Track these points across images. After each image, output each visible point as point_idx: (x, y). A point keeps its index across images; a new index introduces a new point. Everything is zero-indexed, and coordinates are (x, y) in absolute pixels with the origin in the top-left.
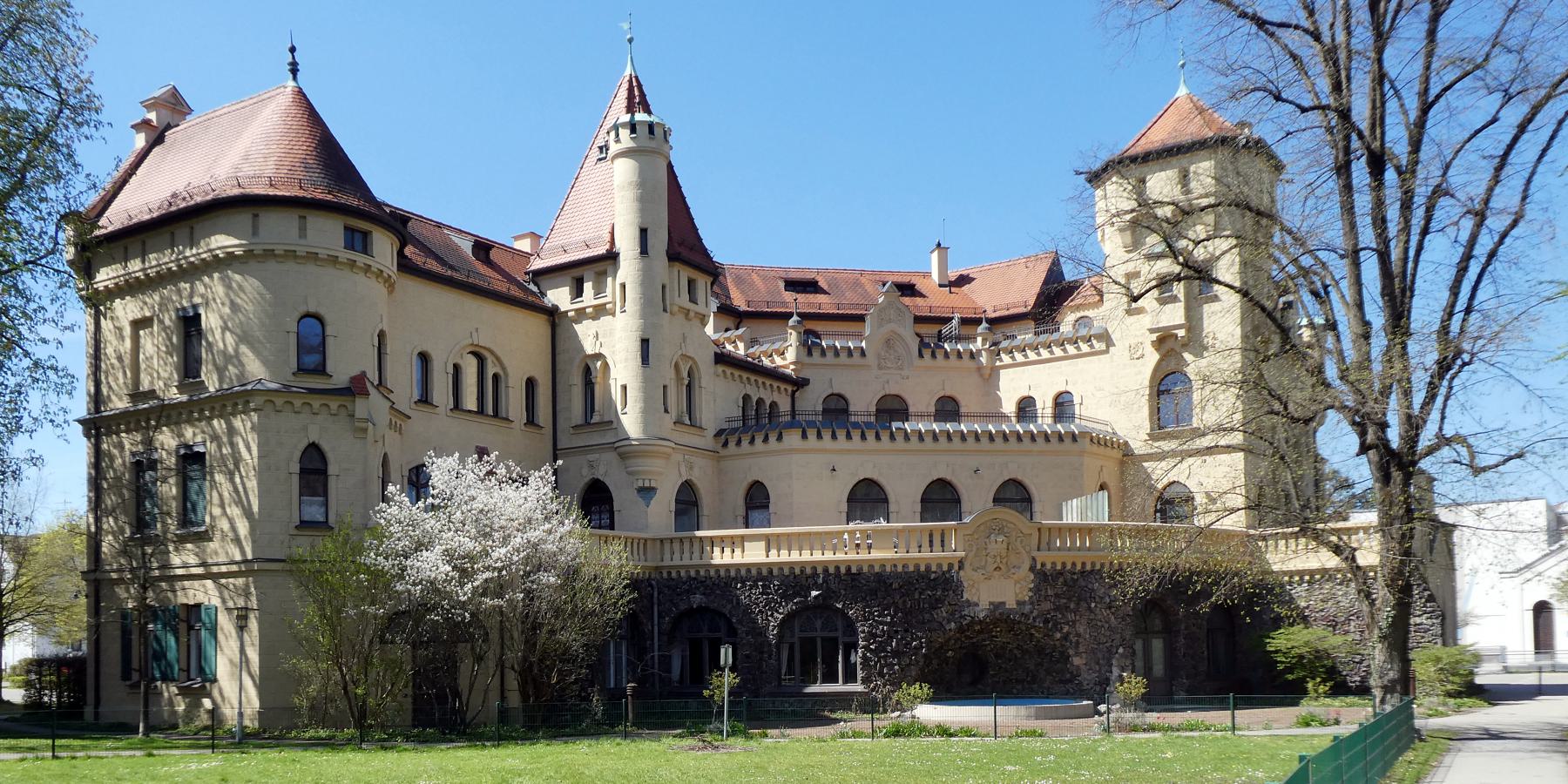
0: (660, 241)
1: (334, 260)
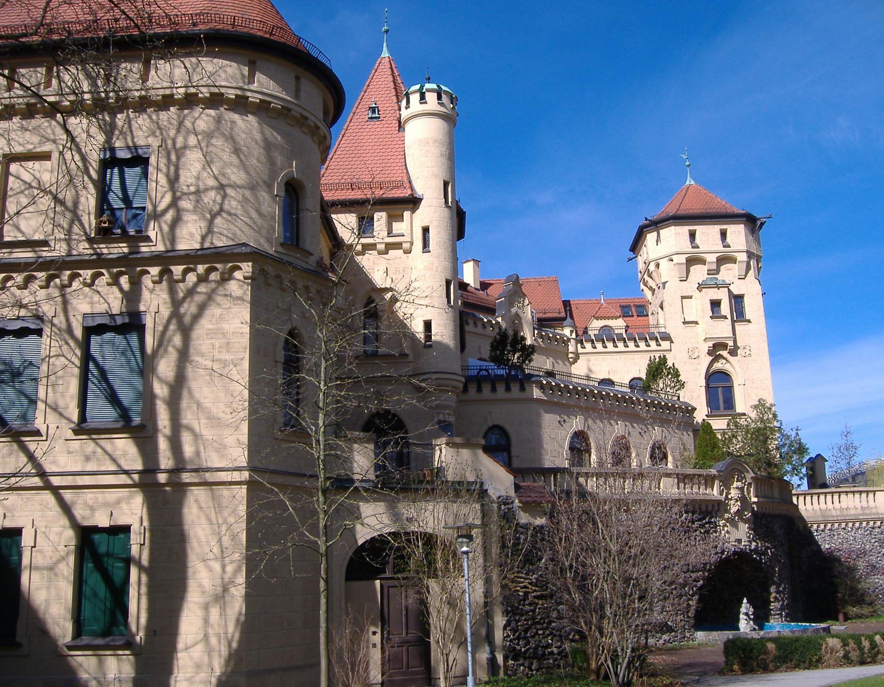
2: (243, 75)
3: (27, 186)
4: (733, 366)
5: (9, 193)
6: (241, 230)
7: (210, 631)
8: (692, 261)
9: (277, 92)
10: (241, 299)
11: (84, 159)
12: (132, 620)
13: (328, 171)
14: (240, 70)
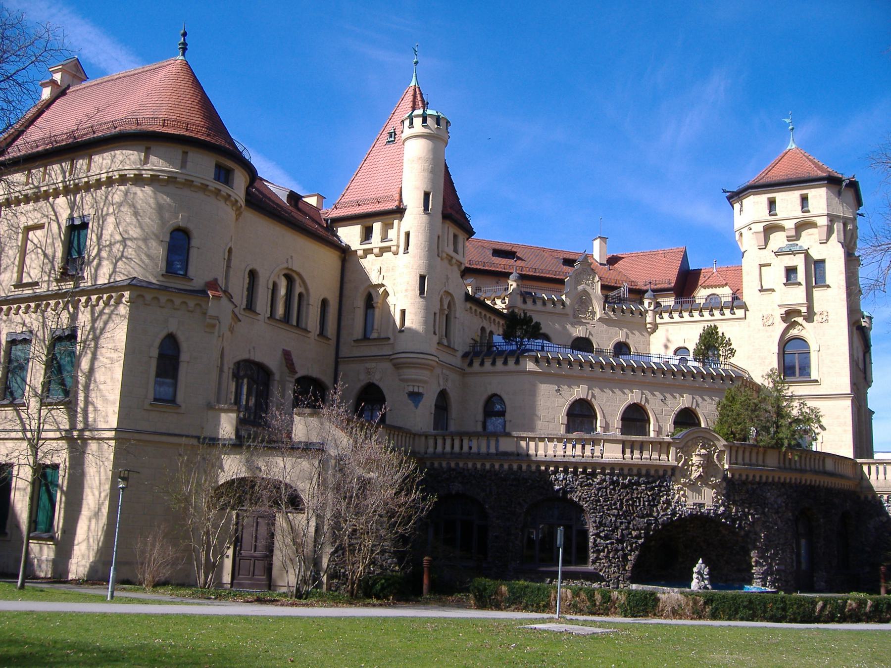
0: (436, 203)
1: (204, 188)
4: (807, 331)
5: (28, 252)
6: (133, 268)
7: (90, 534)
8: (770, 230)
11: (60, 227)
12: (55, 523)
13: (348, 192)
14: (139, 156)
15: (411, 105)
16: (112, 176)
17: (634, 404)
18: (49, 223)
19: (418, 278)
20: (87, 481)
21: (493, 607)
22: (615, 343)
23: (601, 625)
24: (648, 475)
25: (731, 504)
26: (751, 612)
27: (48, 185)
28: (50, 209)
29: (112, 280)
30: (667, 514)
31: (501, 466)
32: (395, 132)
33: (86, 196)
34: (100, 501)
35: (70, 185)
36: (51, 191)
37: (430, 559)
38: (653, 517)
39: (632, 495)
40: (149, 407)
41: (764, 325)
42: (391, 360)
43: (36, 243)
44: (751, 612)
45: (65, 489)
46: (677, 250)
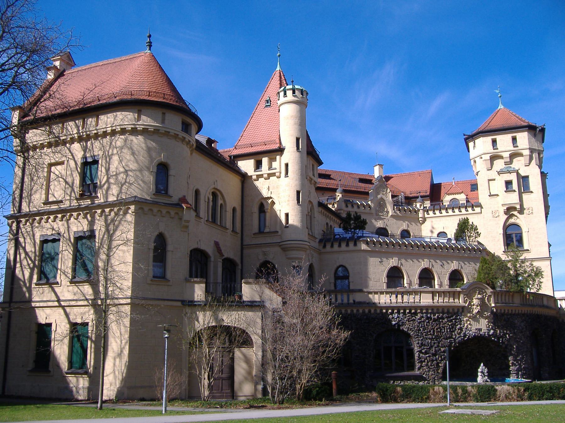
1: (176, 136)
2: (135, 118)
3: (57, 177)
4: (521, 220)
6: (134, 190)
7: (116, 368)
8: (494, 158)
9: (152, 123)
10: (131, 222)
11: (76, 164)
12: (88, 362)
13: (242, 138)
14: (134, 116)
15: (279, 82)
16: (115, 129)
17: (425, 268)
18: (68, 161)
19: (296, 193)
20: (110, 333)
21: (393, 401)
22: (402, 230)
23: (494, 408)
24: (448, 312)
25: (496, 328)
26: (552, 394)
27: (65, 135)
28: (68, 151)
29: (119, 198)
30: (461, 336)
31: (358, 310)
32: (270, 100)
33: (95, 142)
34: (122, 346)
35: (83, 135)
36: (69, 139)
37: (336, 372)
38: (453, 338)
39: (439, 325)
40: (150, 282)
41: (493, 217)
42: (280, 246)
43: (57, 174)
44: (552, 394)
45: (94, 339)
46: (427, 172)
